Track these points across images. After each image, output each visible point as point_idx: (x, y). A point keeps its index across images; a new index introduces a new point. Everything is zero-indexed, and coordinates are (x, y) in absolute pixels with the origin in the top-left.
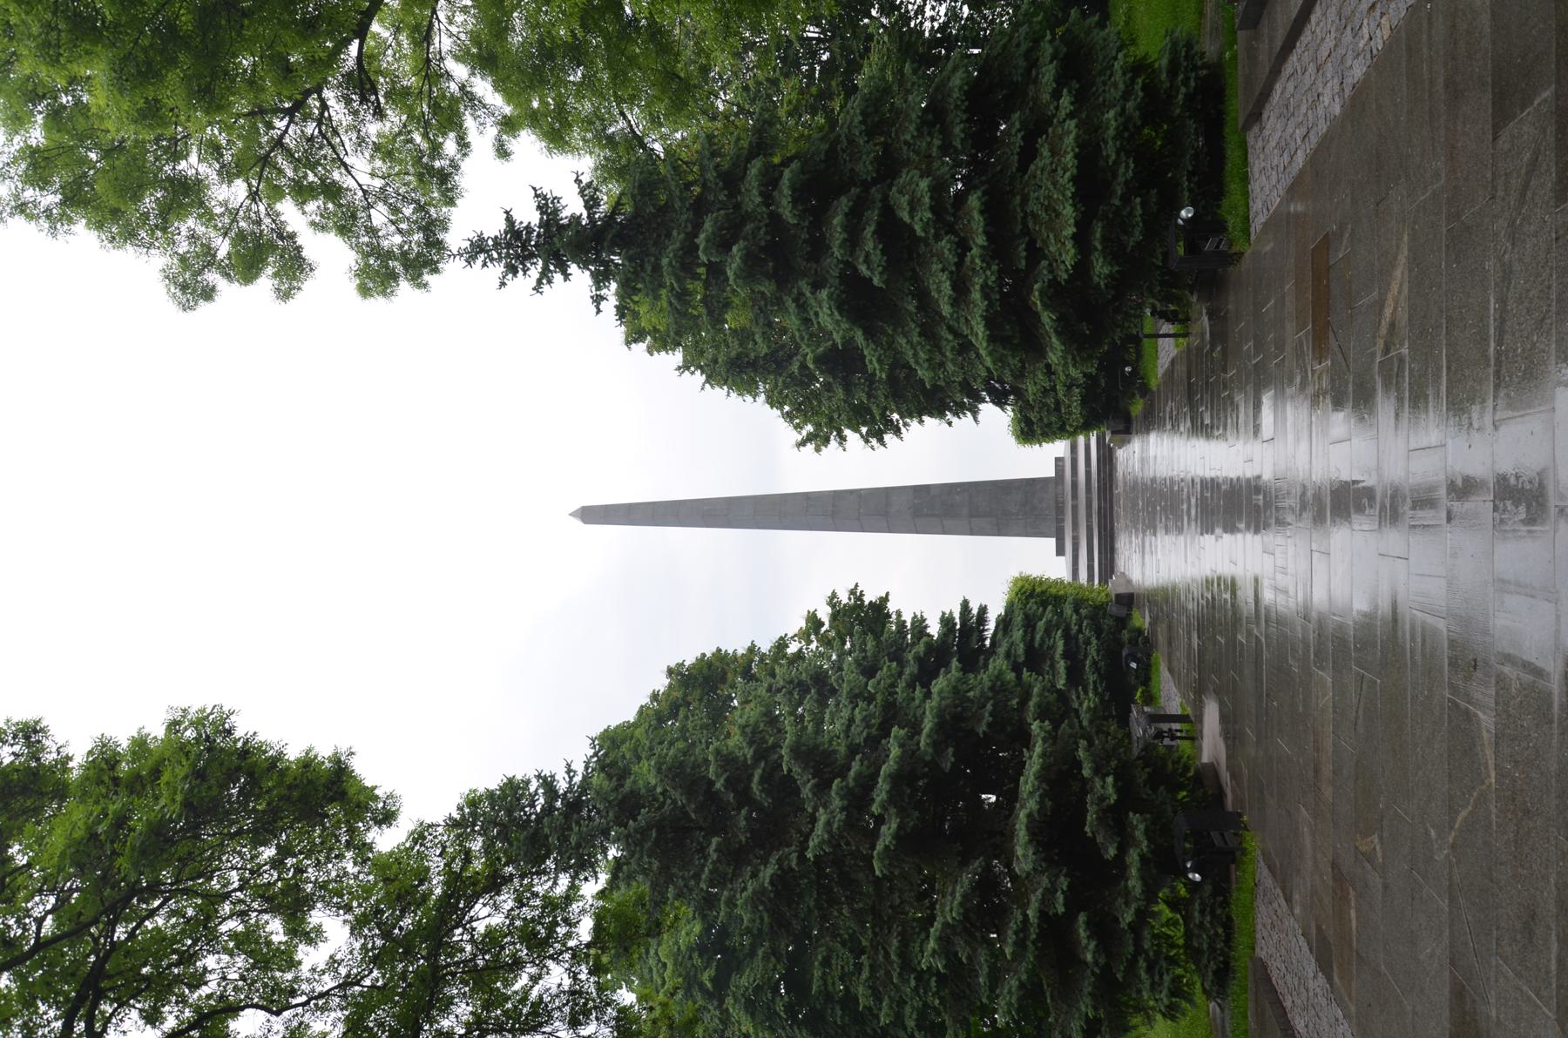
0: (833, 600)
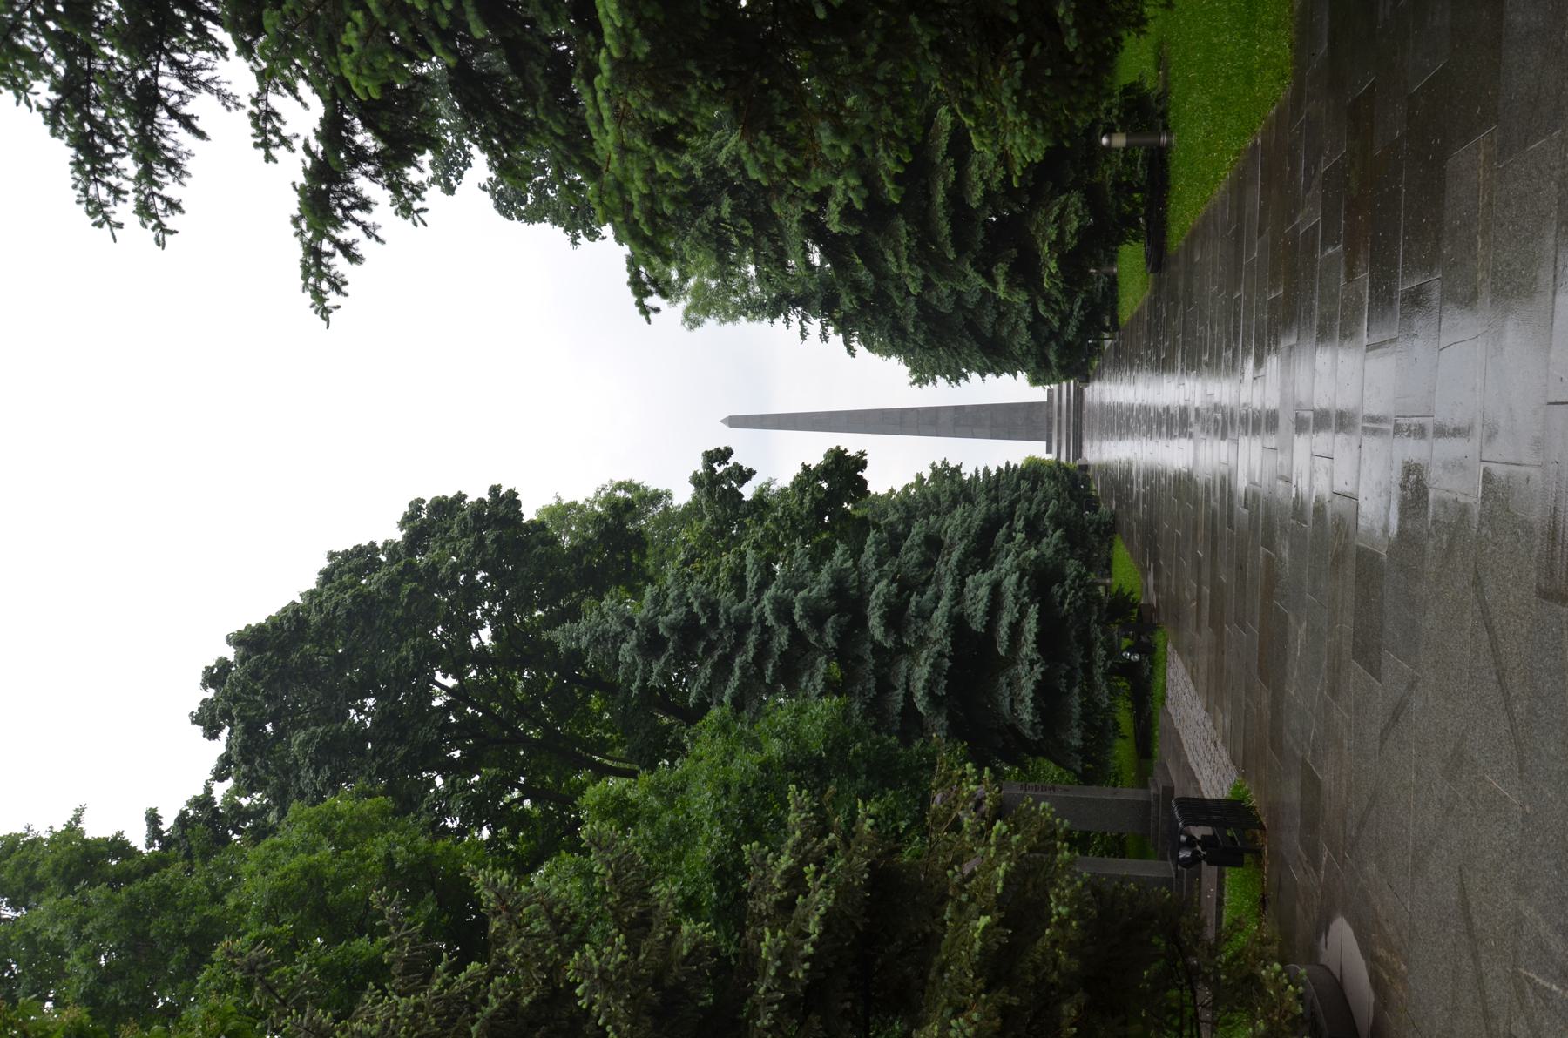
0: (933, 466)
